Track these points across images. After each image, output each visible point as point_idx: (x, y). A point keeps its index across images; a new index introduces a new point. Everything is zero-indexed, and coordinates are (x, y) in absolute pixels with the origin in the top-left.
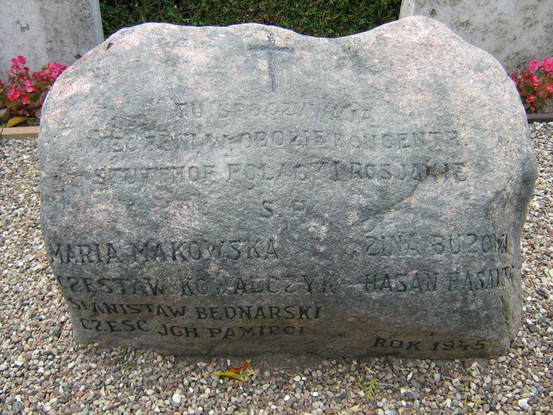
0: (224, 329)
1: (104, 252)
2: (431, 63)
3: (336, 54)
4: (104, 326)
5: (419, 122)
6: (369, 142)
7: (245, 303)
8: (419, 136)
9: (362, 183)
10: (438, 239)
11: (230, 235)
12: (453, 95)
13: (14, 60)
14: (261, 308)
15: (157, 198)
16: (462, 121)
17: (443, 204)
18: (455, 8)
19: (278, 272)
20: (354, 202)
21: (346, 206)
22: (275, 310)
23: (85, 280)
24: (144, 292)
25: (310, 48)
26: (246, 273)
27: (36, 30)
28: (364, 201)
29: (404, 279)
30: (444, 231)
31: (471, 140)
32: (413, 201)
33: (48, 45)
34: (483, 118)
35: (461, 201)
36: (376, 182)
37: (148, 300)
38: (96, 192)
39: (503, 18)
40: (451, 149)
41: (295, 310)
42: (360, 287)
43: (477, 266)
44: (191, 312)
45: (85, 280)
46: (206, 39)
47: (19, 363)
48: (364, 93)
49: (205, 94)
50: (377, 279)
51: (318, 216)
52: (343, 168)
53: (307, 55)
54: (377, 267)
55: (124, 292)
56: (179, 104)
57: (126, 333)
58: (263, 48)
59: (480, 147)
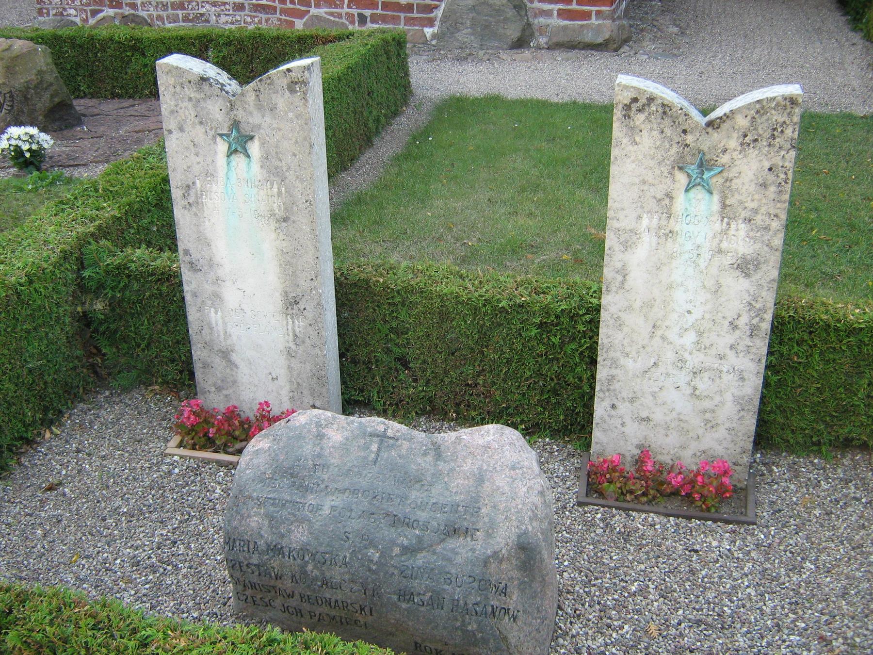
0: (317, 613)
1: (251, 547)
2: (483, 460)
3: (426, 446)
4: (250, 599)
5: (457, 498)
6: (421, 507)
7: (328, 596)
8: (455, 507)
9: (409, 532)
10: (449, 576)
11: (322, 549)
12: (487, 483)
13: (260, 404)
14: (336, 601)
15: (286, 519)
16: (487, 502)
17: (457, 554)
18: (634, 404)
19: (347, 577)
20: (399, 542)
21: (393, 543)
22: (345, 604)
23: (240, 563)
24: (271, 576)
25: (410, 439)
26: (328, 575)
27: (283, 381)
28: (406, 542)
29: (422, 597)
30: (453, 571)
31: (487, 515)
32: (439, 548)
33: (291, 394)
34: (500, 501)
35: (470, 554)
36: (417, 532)
37: (272, 583)
38: (255, 509)
39: (682, 417)
40: (473, 519)
41: (357, 607)
42: (395, 598)
43: (472, 600)
44: (297, 596)
45: (240, 563)
46: (345, 425)
47: (195, 615)
48: (433, 474)
49: (333, 461)
50: (406, 595)
51: (375, 547)
52: (399, 519)
53: (406, 444)
54: (407, 586)
55: (260, 575)
56: (315, 465)
57: (262, 608)
58: (378, 436)
59: (491, 521)
